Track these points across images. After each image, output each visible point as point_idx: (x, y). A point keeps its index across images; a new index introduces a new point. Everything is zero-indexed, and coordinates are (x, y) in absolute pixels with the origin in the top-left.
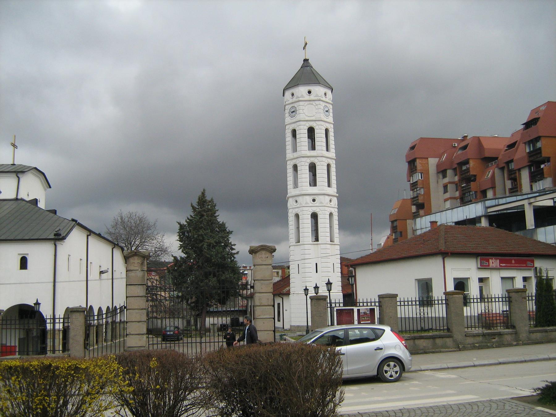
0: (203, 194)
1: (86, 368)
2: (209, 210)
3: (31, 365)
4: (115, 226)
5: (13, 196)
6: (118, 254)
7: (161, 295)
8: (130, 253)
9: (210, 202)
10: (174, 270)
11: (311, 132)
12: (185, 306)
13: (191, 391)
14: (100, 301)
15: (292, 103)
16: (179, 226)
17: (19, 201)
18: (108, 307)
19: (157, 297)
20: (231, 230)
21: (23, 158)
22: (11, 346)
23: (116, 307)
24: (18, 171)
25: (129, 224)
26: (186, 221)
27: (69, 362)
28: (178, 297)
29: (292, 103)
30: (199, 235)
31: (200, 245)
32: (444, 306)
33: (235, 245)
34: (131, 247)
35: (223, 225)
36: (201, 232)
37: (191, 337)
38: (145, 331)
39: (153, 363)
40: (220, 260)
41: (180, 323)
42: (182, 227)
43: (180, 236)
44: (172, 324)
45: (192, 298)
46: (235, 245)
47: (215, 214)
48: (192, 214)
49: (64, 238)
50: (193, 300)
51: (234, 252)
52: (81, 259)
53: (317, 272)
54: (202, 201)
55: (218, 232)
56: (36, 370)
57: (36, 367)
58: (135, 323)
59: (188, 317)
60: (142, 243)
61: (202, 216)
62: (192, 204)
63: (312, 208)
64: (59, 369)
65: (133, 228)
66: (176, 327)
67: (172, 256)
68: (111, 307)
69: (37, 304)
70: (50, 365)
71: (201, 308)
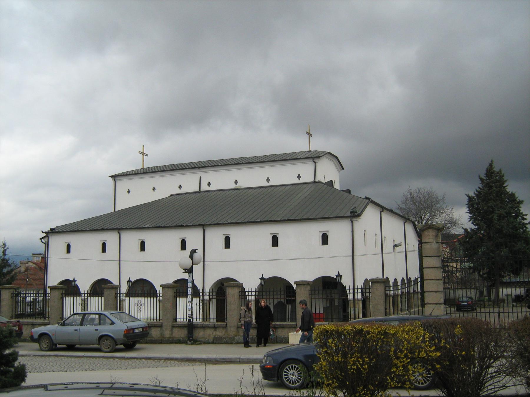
0: (491, 165)
1: (395, 333)
2: (497, 181)
3: (345, 330)
4: (405, 202)
5: (311, 180)
6: (410, 229)
7: (452, 266)
8: (424, 226)
9: (498, 173)
10: (465, 242)
12: (477, 277)
13: (496, 359)
14: (395, 272)
16: (467, 198)
17: (317, 184)
18: (403, 279)
19: (448, 269)
20: (521, 200)
21: (318, 144)
22: (319, 314)
23: (410, 278)
24: (313, 157)
25: (418, 199)
26: (475, 194)
27: (379, 327)
28: (470, 268)
30: (488, 207)
31: (490, 217)
32: (178, 317)
33: (526, 215)
34: (422, 221)
35: (513, 195)
36: (490, 204)
37: (484, 307)
38: (442, 301)
39: (458, 331)
40: (511, 231)
41: (473, 294)
42: (470, 199)
43: (469, 207)
44: (464, 295)
45: (483, 269)
46: (526, 215)
47: (503, 184)
48: (481, 186)
49: (359, 215)
50: (485, 271)
51: (525, 222)
52: (376, 234)
54: (490, 172)
55: (508, 202)
56: (349, 334)
57: (349, 331)
58: (432, 293)
59: (481, 288)
60: (432, 217)
61: (491, 187)
62: (479, 176)
64: (370, 334)
65: (422, 203)
66: (470, 298)
67: (463, 228)
68: (405, 279)
69: (339, 276)
70: (362, 330)
71: (494, 280)
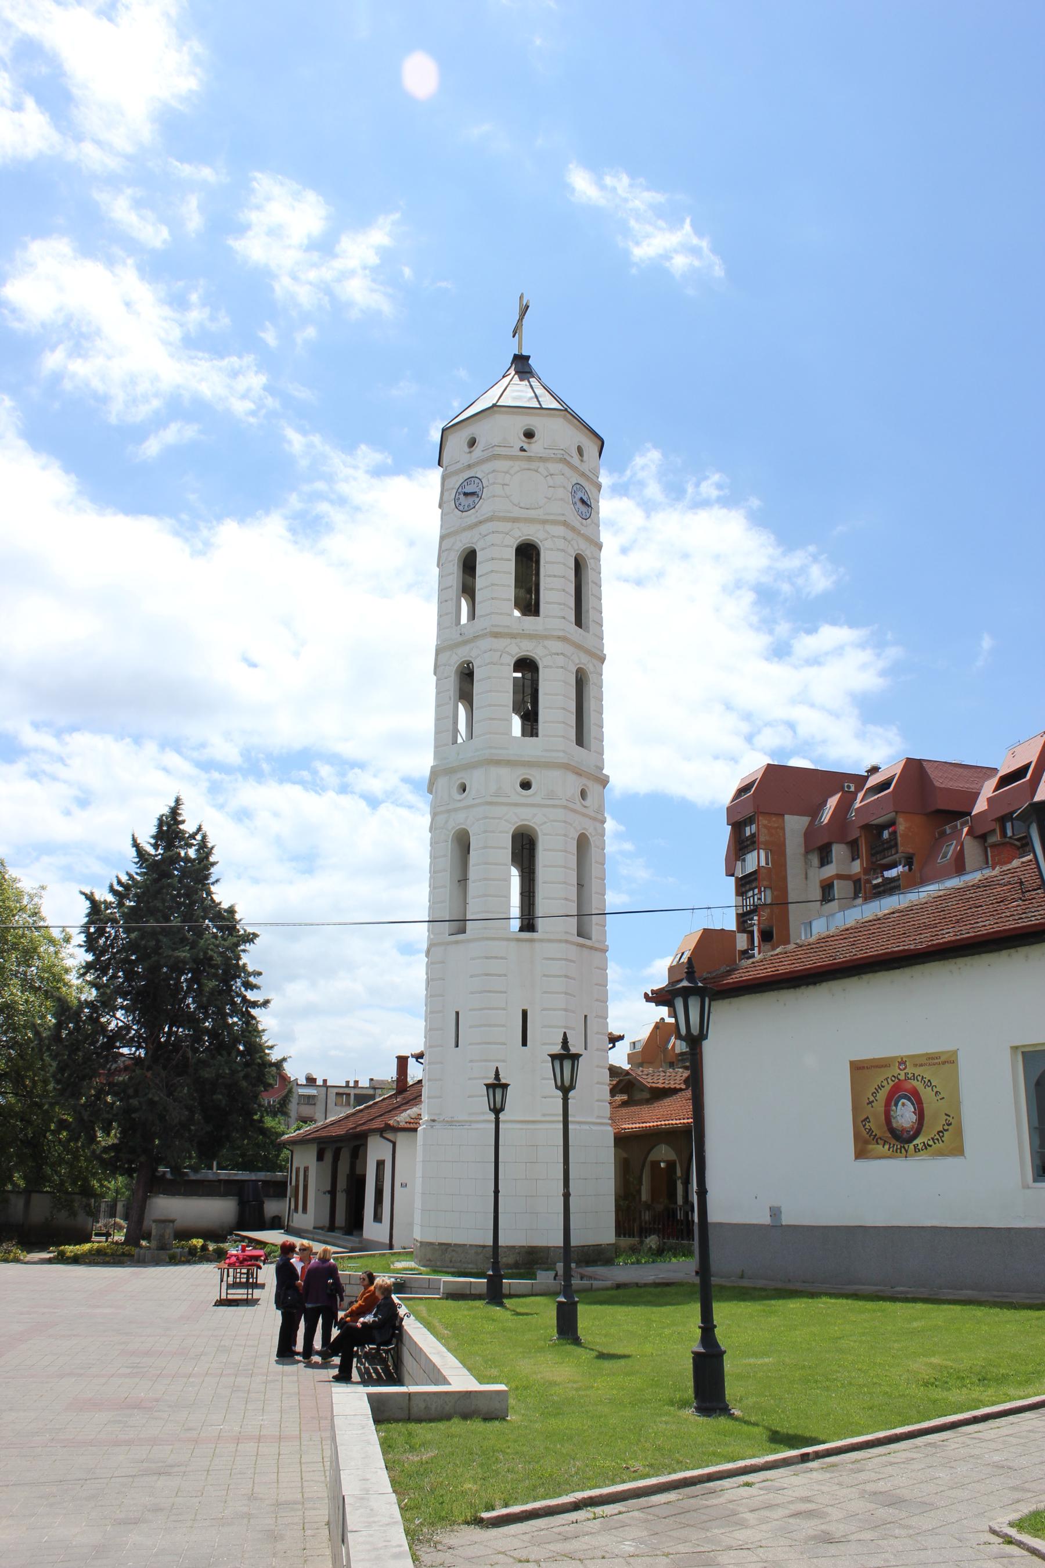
0: (174, 812)
11: (527, 555)
15: (469, 466)
16: (88, 904)
26: (112, 890)
29: (469, 466)
53: (524, 1043)
62: (134, 840)
63: (519, 810)
